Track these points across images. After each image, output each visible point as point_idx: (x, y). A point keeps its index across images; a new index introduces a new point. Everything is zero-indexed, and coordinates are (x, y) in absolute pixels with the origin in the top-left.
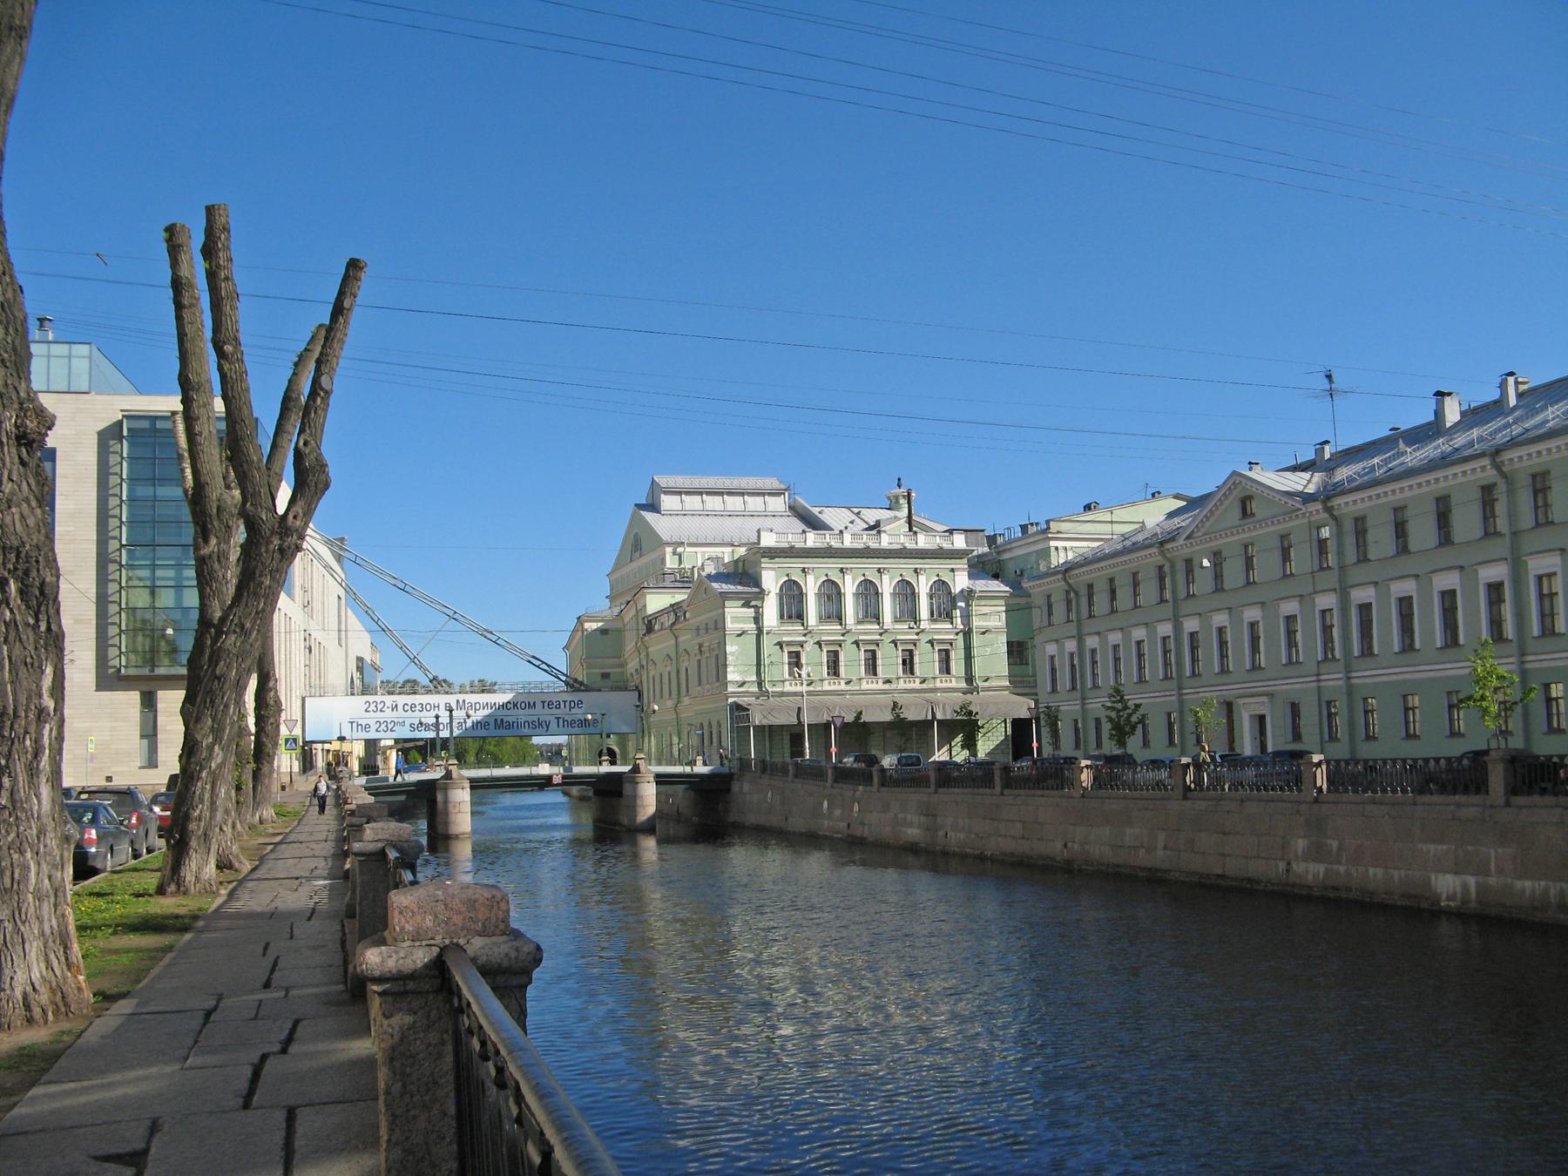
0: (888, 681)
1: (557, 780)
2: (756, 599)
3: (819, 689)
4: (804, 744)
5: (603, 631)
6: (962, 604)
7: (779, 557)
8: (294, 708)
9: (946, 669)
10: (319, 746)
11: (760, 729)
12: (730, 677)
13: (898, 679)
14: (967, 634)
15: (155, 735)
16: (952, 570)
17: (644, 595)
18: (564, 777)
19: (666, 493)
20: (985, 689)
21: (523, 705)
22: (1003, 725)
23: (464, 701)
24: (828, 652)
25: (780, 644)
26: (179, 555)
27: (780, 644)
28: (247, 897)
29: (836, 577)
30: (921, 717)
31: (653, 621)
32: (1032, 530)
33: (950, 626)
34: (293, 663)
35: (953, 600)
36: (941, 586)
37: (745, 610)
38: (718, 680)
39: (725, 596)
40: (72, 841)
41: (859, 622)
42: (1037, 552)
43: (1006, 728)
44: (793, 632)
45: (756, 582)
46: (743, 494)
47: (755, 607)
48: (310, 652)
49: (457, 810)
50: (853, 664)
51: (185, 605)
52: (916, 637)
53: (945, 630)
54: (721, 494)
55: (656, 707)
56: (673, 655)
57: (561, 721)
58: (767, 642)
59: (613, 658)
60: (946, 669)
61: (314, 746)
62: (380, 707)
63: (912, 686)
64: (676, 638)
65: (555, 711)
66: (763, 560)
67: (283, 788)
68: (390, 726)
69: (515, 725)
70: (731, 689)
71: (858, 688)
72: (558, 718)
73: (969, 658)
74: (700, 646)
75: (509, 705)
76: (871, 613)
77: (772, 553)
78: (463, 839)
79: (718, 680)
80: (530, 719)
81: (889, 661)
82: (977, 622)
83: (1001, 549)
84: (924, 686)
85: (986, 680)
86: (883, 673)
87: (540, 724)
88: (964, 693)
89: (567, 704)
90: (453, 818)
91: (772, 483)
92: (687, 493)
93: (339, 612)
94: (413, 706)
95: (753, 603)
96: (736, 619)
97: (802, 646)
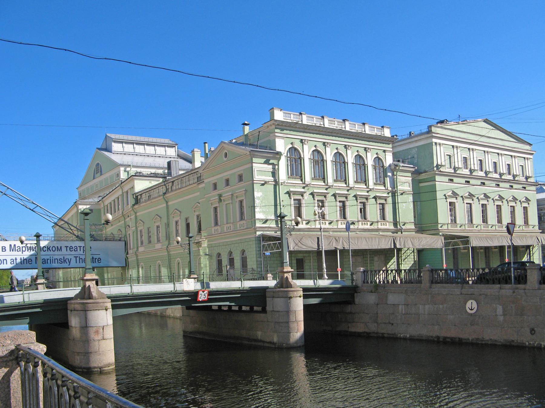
2: (274, 158)
3: (313, 227)
7: (287, 130)
9: (383, 217)
11: (326, 252)
13: (358, 221)
14: (394, 194)
16: (384, 151)
17: (133, 180)
19: (115, 142)
21: (54, 249)
23: (15, 245)
25: (288, 193)
27: (288, 193)
30: (388, 247)
31: (139, 197)
36: (378, 160)
37: (266, 166)
40: (398, 163)
41: (335, 181)
42: (417, 147)
44: (296, 185)
45: (271, 146)
46: (154, 145)
47: (273, 164)
49: (100, 337)
56: (164, 215)
57: (78, 259)
58: (282, 190)
64: (167, 202)
65: (73, 253)
66: (276, 131)
69: (49, 261)
70: (258, 224)
71: (336, 227)
72: (76, 257)
74: (220, 196)
75: (45, 249)
77: (283, 126)
78: (108, 373)
79: (216, 224)
80: (58, 257)
84: (372, 227)
85: (404, 225)
87: (65, 261)
88: (393, 233)
91: (167, 141)
92: (126, 143)
95: (271, 161)
96: (261, 172)
97: (302, 196)
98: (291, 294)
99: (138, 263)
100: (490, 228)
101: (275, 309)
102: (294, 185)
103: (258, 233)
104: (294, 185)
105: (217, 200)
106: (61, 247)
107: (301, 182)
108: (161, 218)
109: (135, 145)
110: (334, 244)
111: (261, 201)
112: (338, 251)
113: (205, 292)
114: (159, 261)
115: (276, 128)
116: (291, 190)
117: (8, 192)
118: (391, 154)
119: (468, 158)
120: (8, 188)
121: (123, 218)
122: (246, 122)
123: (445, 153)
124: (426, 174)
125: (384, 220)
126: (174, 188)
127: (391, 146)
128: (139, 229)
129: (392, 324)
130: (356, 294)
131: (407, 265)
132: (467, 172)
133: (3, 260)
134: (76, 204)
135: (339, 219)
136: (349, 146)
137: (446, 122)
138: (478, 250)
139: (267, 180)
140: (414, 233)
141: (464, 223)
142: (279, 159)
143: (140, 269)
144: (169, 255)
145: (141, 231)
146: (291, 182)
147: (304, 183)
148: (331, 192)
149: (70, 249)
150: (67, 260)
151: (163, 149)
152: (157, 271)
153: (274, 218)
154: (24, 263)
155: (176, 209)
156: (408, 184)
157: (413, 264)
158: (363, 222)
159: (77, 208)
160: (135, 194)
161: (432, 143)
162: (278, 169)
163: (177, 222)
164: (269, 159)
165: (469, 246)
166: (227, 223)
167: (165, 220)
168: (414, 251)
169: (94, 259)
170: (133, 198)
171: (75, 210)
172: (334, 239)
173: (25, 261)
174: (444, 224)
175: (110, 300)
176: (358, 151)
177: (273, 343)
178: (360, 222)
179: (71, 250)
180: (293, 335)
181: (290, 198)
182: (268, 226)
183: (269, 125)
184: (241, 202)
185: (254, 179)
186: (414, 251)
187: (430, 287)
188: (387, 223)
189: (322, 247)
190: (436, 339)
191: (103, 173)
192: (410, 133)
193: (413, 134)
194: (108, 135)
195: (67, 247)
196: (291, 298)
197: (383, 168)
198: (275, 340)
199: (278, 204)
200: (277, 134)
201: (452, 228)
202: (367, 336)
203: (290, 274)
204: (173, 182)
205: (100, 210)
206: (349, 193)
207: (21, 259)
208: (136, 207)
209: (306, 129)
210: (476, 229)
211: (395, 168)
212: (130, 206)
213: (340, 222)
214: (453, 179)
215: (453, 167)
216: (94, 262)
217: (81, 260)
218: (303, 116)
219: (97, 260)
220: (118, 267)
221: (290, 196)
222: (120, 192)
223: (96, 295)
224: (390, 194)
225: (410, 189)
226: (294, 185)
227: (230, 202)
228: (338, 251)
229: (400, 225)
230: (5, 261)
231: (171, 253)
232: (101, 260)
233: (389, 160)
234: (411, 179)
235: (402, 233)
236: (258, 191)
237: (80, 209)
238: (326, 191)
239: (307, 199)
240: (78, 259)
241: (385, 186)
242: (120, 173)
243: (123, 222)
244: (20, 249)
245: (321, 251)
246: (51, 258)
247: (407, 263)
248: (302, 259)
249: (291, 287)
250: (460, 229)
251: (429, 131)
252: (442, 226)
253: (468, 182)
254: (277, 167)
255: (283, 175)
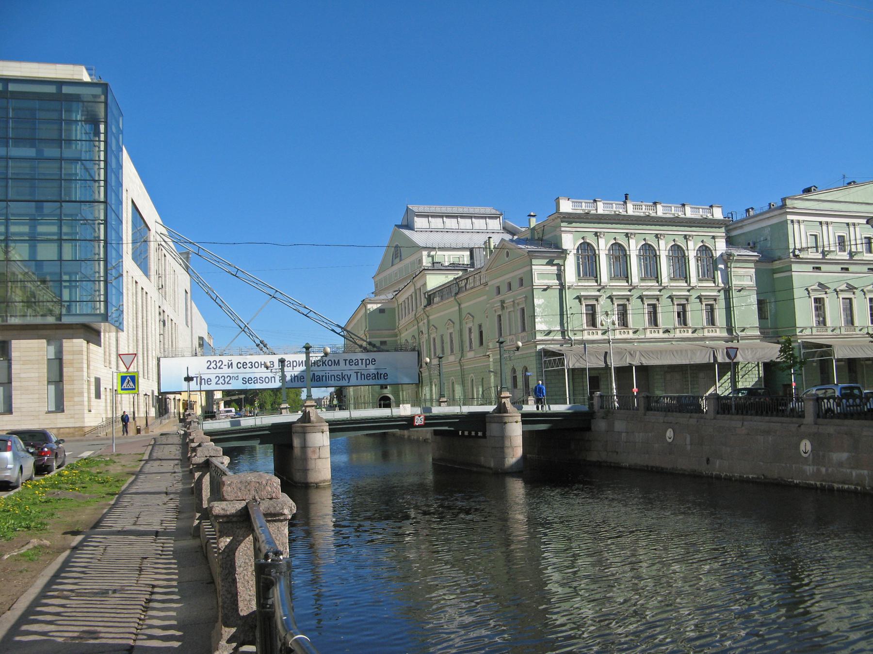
0: (667, 331)
1: (419, 421)
2: (558, 258)
4: (611, 384)
5: (381, 311)
6: (722, 266)
7: (576, 222)
8: (150, 366)
9: (712, 321)
10: (172, 396)
11: (616, 369)
12: (539, 327)
13: (675, 329)
14: (727, 291)
15: (10, 382)
16: (714, 237)
17: (425, 275)
18: (426, 418)
19: (418, 216)
20: (743, 338)
21: (330, 362)
22: (757, 368)
24: (618, 305)
25: (579, 298)
26: (33, 211)
27: (579, 298)
28: (139, 484)
29: (622, 241)
32: (752, 213)
33: (714, 285)
34: (149, 329)
35: (715, 263)
36: (704, 250)
37: (549, 267)
38: (524, 330)
39: (531, 255)
42: (770, 226)
43: (759, 371)
44: (589, 288)
45: (556, 244)
46: (471, 217)
47: (558, 265)
48: (164, 325)
49: (316, 456)
50: (638, 316)
51: (39, 258)
52: (687, 293)
53: (709, 288)
54: (456, 217)
55: (520, 344)
56: (456, 320)
57: (359, 374)
58: (569, 296)
59: (389, 330)
60: (712, 321)
61: (168, 396)
62: (218, 365)
63: (685, 335)
64: (460, 305)
65: (354, 367)
66: (562, 224)
67: (138, 431)
68: (227, 380)
69: (324, 378)
71: (643, 337)
72: (357, 373)
73: (729, 309)
74: (503, 302)
76: (652, 271)
77: (570, 218)
78: (324, 488)
79: (524, 330)
80: (335, 373)
81: (667, 315)
82: (735, 282)
83: (731, 227)
84: (695, 335)
85: (743, 331)
86: (663, 324)
87: (343, 377)
88: (727, 342)
89: (364, 361)
90: (312, 464)
91: (489, 210)
92: (433, 216)
93: (187, 315)
94: (244, 364)
95: (556, 262)
96: (542, 275)
97: (597, 300)
98: (506, 420)
99: (431, 379)
100: (857, 332)
101: (492, 435)
102: (586, 287)
103: (539, 347)
104: (586, 288)
105: (500, 307)
106: (339, 360)
107: (596, 284)
108: (473, 316)
109: (444, 218)
110: (627, 360)
111: (543, 310)
112: (634, 367)
113: (422, 417)
114: (452, 378)
115: (562, 222)
116: (583, 293)
117: (277, 295)
118: (724, 240)
119: (847, 238)
120: (277, 291)
121: (416, 322)
122: (532, 214)
123: (808, 234)
124: (780, 261)
125: (714, 325)
126: (468, 287)
127: (723, 230)
128: (432, 336)
129: (617, 453)
130: (592, 420)
131: (748, 384)
132: (845, 256)
133: (271, 378)
134: (364, 303)
135: (647, 327)
136: (661, 234)
137: (814, 190)
138: (862, 362)
139: (551, 284)
140: (759, 341)
141: (838, 326)
142: (565, 259)
143: (434, 386)
144: (462, 370)
145: (434, 339)
146: (583, 284)
147: (600, 285)
148: (636, 293)
149: (349, 362)
150: (346, 377)
151: (483, 221)
152: (451, 389)
153: (559, 329)
154: (295, 381)
155: (469, 313)
156: (750, 277)
157: (756, 382)
158: (682, 329)
159: (366, 307)
160: (427, 292)
161: (786, 221)
162: (564, 270)
163: (470, 330)
164: (553, 259)
165: (832, 357)
166: (510, 335)
167: (457, 326)
168: (758, 365)
169: (379, 375)
170: (425, 297)
171: (363, 311)
172: (627, 354)
173: (296, 378)
174: (805, 328)
175: (328, 424)
176: (674, 240)
177: (490, 468)
178: (678, 330)
179: (351, 364)
180: (508, 460)
181: (581, 304)
182: (552, 338)
183: (554, 218)
184: (523, 310)
185: (534, 284)
186: (758, 365)
187: (645, 415)
188: (718, 330)
189: (611, 363)
190: (646, 469)
191: (403, 258)
192: (770, 204)
193: (773, 205)
194: (410, 207)
195: (345, 360)
196: (506, 423)
197: (713, 259)
198: (492, 465)
199: (565, 313)
200: (563, 229)
201: (818, 333)
202: (599, 465)
203: (508, 399)
204: (467, 279)
205: (394, 309)
206: (661, 294)
207: (291, 376)
208: (428, 308)
209: (601, 219)
210: (859, 332)
211: (728, 258)
212: (423, 307)
213: (648, 330)
214: (820, 267)
215: (820, 250)
216: (379, 378)
217: (363, 376)
218: (598, 203)
219: (382, 376)
220: (412, 384)
221: (580, 301)
222: (412, 290)
223: (315, 420)
224: (722, 292)
225: (752, 283)
226: (586, 288)
227: (512, 309)
228: (634, 367)
229: (735, 331)
230: (273, 379)
231: (464, 367)
232: (387, 376)
233: (720, 247)
234: (754, 270)
235: (738, 342)
236: (539, 298)
237: (369, 309)
238: (629, 293)
239: (603, 305)
240: (359, 374)
241: (714, 282)
242: (422, 258)
243: (416, 326)
244: (290, 363)
245: (610, 369)
246: (327, 374)
247: (748, 380)
248: (597, 377)
249: (507, 413)
250: (831, 333)
251: (784, 206)
252: (803, 330)
253: (847, 269)
254: (563, 267)
255: (571, 275)
